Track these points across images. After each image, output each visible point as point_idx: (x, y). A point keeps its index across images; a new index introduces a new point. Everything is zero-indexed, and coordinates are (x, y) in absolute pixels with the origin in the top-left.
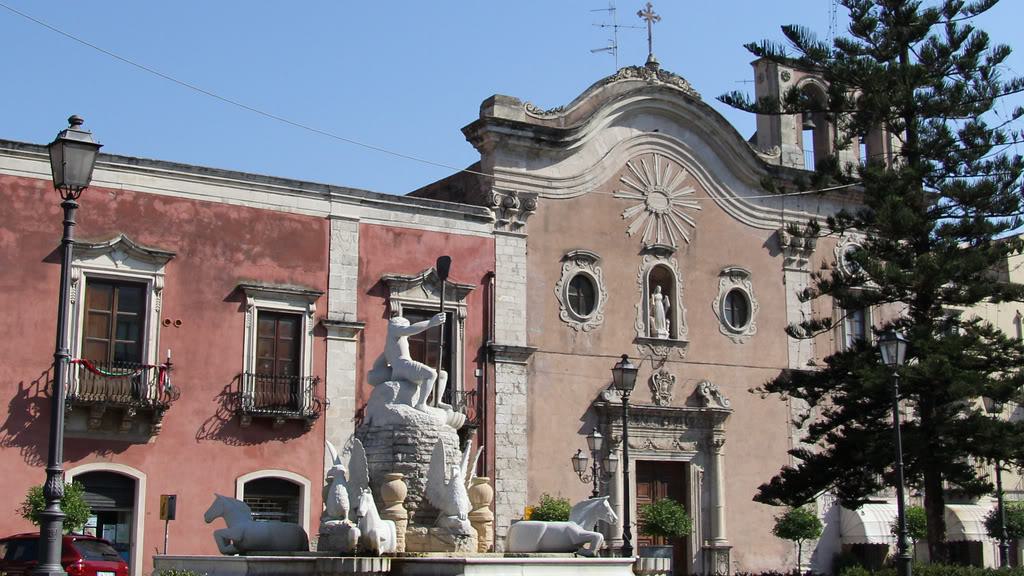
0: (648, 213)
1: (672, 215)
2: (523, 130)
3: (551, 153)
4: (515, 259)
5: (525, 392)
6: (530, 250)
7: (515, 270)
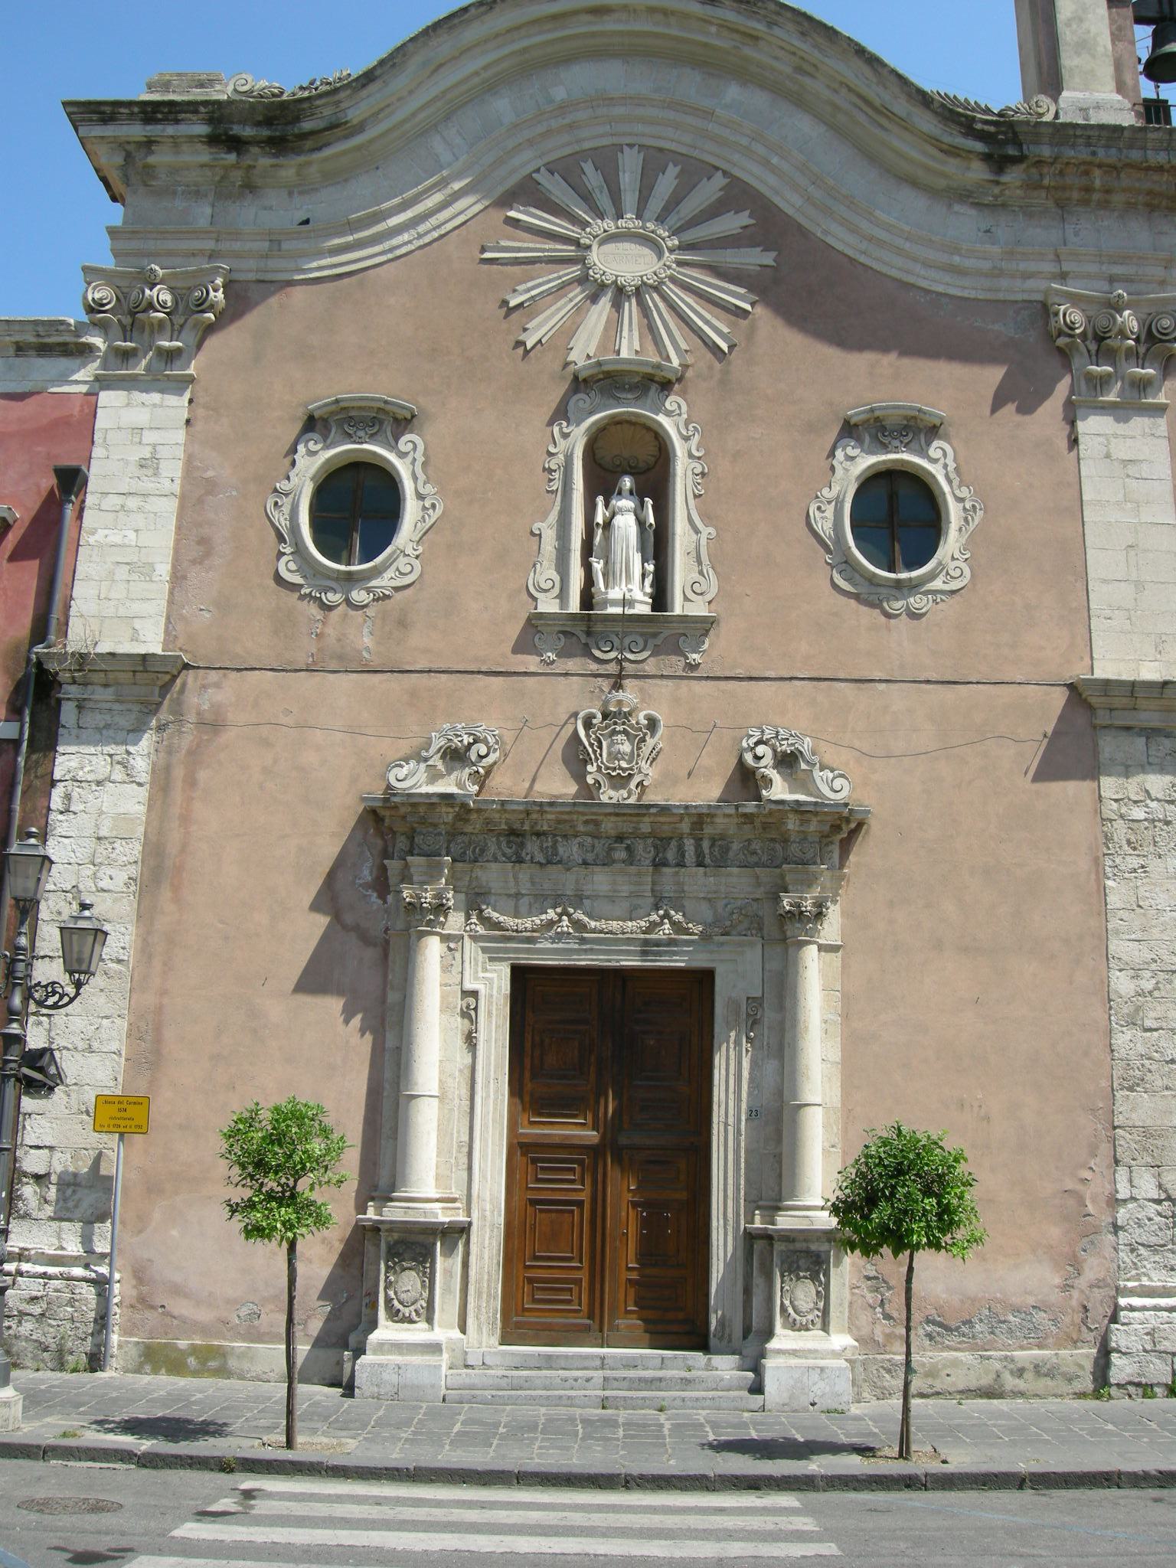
0: (605, 302)
1: (673, 291)
2: (177, 122)
3: (283, 173)
4: (149, 437)
5: (144, 778)
6: (201, 412)
7: (149, 465)
